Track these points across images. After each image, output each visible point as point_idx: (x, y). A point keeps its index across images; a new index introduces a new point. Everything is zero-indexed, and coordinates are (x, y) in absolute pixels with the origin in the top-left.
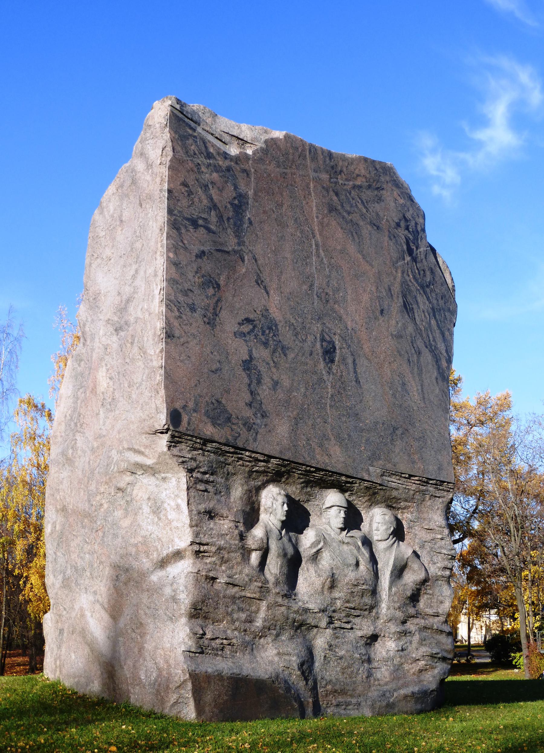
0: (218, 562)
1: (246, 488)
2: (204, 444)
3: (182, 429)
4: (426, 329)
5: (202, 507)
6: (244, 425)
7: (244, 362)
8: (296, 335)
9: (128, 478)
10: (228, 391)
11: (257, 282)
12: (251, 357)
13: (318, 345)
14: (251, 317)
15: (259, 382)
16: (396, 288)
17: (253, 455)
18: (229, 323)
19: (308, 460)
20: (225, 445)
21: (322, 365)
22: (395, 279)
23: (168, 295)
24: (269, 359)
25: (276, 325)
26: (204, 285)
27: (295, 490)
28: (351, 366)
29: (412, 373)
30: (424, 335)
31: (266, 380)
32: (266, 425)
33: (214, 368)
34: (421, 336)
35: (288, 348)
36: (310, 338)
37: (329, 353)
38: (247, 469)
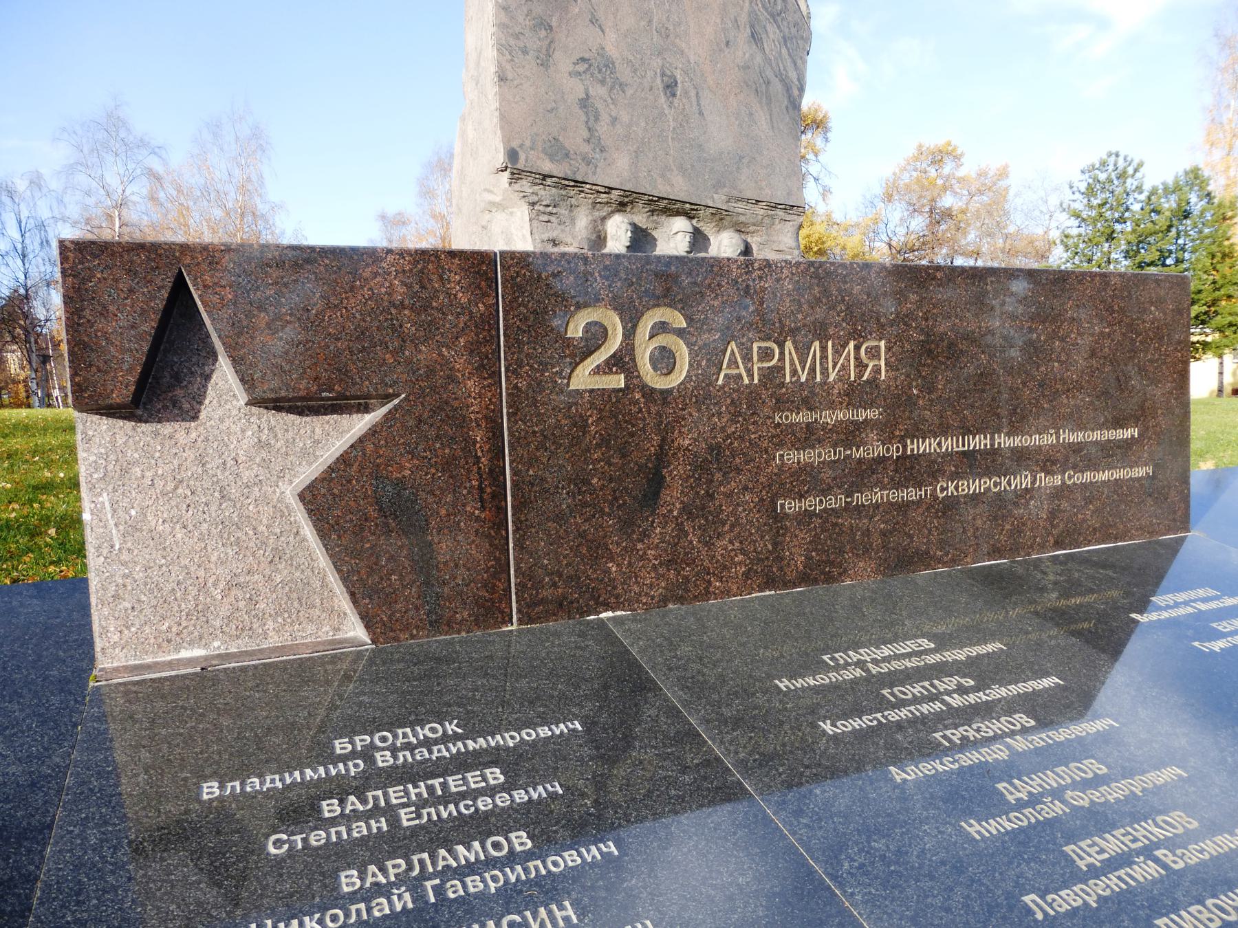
2: (544, 179)
3: (519, 166)
4: (776, 59)
5: (545, 236)
6: (583, 160)
8: (635, 71)
9: (487, 216)
10: (565, 129)
11: (591, 21)
14: (586, 56)
15: (597, 119)
16: (744, 19)
18: (563, 63)
21: (663, 99)
22: (742, 9)
23: (498, 39)
24: (606, 96)
25: (613, 63)
26: (535, 28)
27: (641, 219)
28: (694, 99)
29: (760, 103)
30: (774, 65)
31: (605, 118)
36: (650, 74)
37: (670, 87)
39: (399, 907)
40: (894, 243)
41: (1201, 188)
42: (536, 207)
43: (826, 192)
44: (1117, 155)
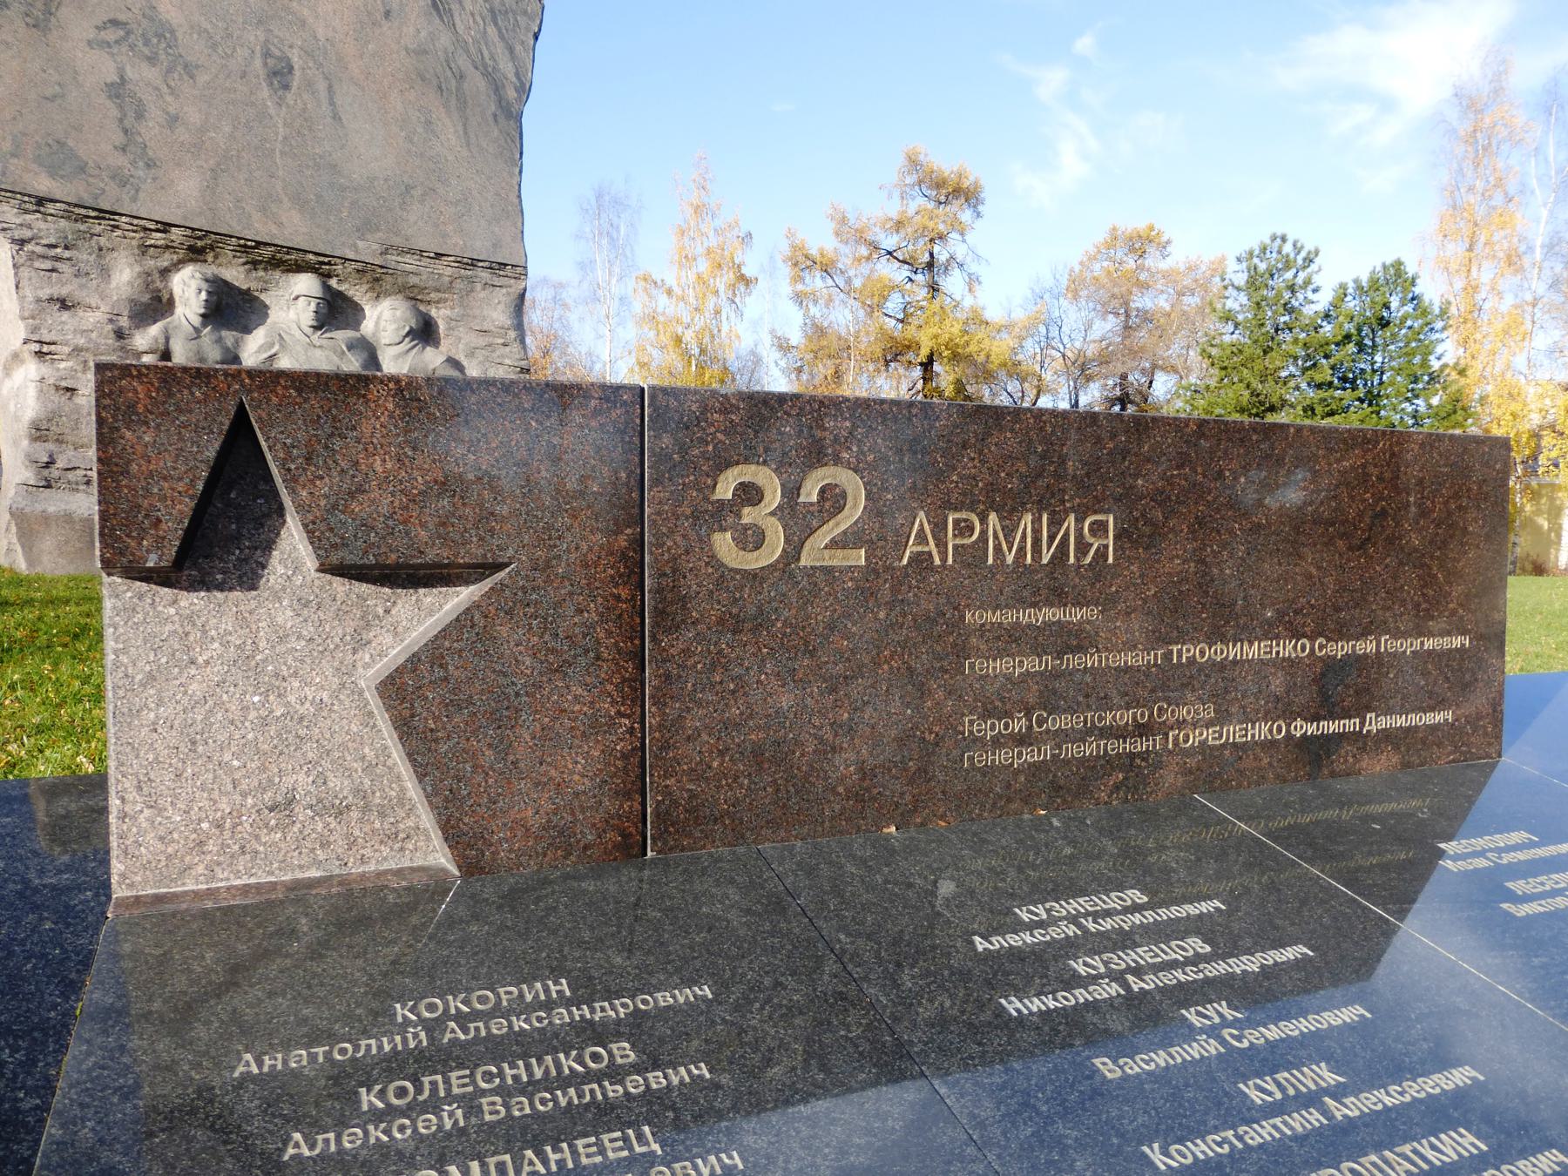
0: (79, 368)
1: (137, 269)
5: (45, 293)
7: (110, 86)
8: (214, 46)
12: (122, 78)
13: (258, 63)
14: (122, 17)
15: (140, 116)
17: (135, 222)
19: (237, 230)
20: (76, 206)
21: (265, 92)
24: (159, 82)
25: (172, 32)
27: (235, 274)
28: (323, 95)
30: (472, 50)
31: (154, 113)
32: (154, 179)
33: (49, 92)
34: (467, 51)
35: (197, 67)
36: (242, 53)
37: (280, 75)
38: (134, 243)
39: (412, 1045)
40: (1069, 354)
41: (1405, 290)
42: (29, 247)
43: (973, 282)
44: (1284, 239)
